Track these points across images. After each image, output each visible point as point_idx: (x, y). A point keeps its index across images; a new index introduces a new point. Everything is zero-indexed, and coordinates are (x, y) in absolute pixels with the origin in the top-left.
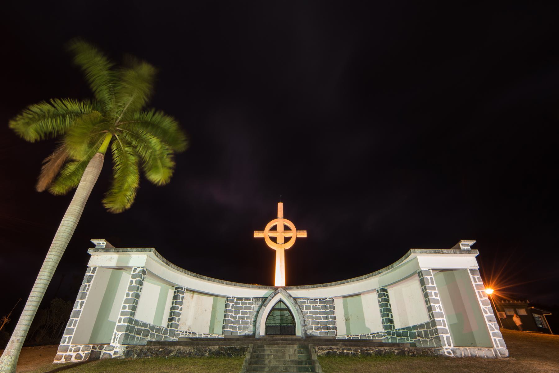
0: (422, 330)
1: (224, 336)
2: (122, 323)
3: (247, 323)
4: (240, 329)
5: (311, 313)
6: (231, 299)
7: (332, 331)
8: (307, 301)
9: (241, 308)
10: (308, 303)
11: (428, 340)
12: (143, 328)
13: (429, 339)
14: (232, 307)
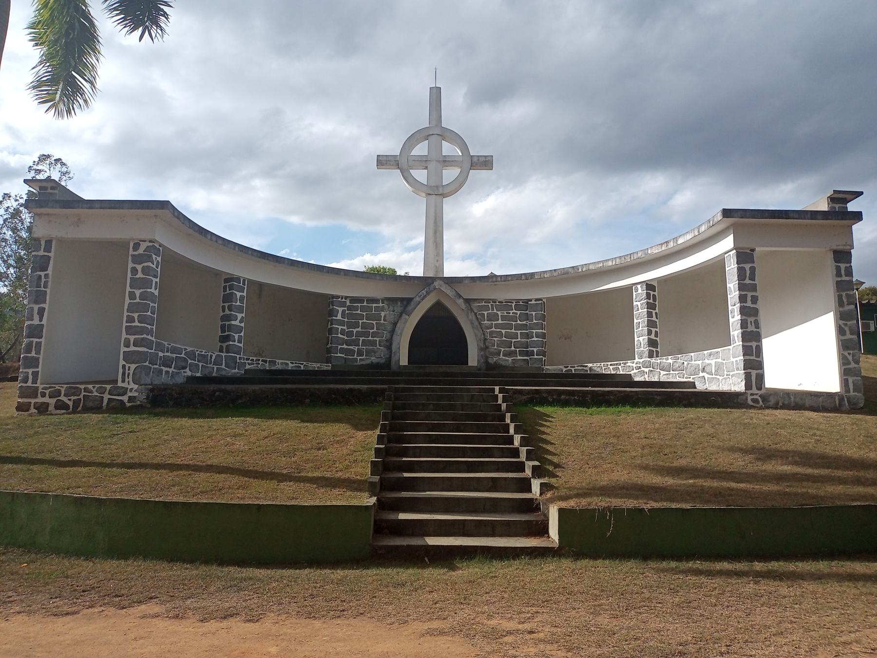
0: (713, 362)
3: (373, 343)
4: (360, 353)
5: (497, 326)
6: (340, 299)
10: (493, 310)
11: (721, 378)
12: (174, 355)
14: (343, 315)
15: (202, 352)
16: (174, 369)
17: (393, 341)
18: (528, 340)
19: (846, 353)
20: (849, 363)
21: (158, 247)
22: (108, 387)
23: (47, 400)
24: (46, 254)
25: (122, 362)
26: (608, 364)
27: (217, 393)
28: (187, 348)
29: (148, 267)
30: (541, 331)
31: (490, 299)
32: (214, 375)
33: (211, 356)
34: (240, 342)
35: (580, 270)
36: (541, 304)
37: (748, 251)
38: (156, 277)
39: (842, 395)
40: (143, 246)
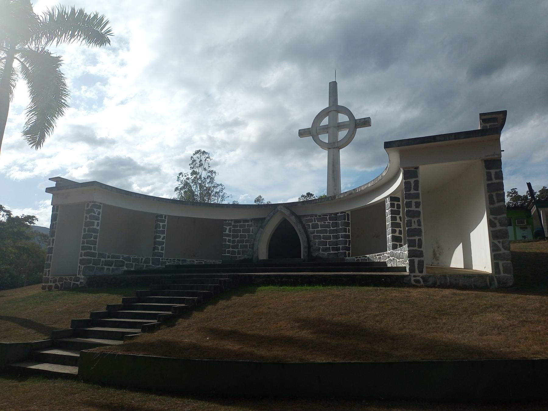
2: (84, 257)
3: (246, 247)
4: (239, 253)
5: (318, 232)
6: (227, 222)
8: (314, 218)
10: (315, 221)
12: (114, 260)
14: (230, 231)
15: (135, 257)
16: (114, 266)
19: (496, 242)
20: (500, 250)
21: (99, 204)
22: (73, 277)
23: (52, 284)
24: (416, 192)
25: (79, 265)
26: (376, 255)
30: (345, 233)
31: (313, 215)
32: (144, 269)
33: (142, 259)
34: (162, 250)
36: (345, 215)
37: (413, 169)
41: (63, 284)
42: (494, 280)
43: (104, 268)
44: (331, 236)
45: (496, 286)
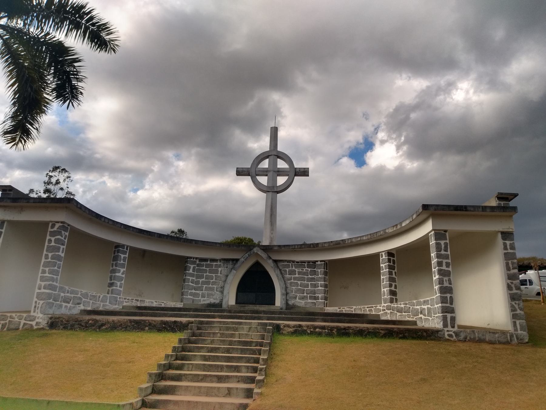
0: (426, 307)
1: (183, 303)
2: (43, 290)
3: (212, 289)
4: (203, 296)
5: (295, 279)
7: (320, 302)
9: (205, 271)
10: (292, 267)
11: (431, 319)
12: (72, 295)
13: (432, 317)
14: (194, 270)
15: (93, 293)
16: (72, 304)
17: (224, 288)
18: (316, 289)
19: (513, 303)
20: (515, 310)
21: (67, 226)
22: (25, 315)
25: (35, 299)
26: (365, 307)
27: (90, 322)
28: (82, 290)
29: (58, 239)
34: (121, 287)
35: (347, 242)
37: (443, 232)
38: (63, 244)
39: (512, 333)
40: (57, 225)
41: (6, 323)
42: (514, 337)
43: (62, 305)
44: (308, 284)
45: (516, 342)
